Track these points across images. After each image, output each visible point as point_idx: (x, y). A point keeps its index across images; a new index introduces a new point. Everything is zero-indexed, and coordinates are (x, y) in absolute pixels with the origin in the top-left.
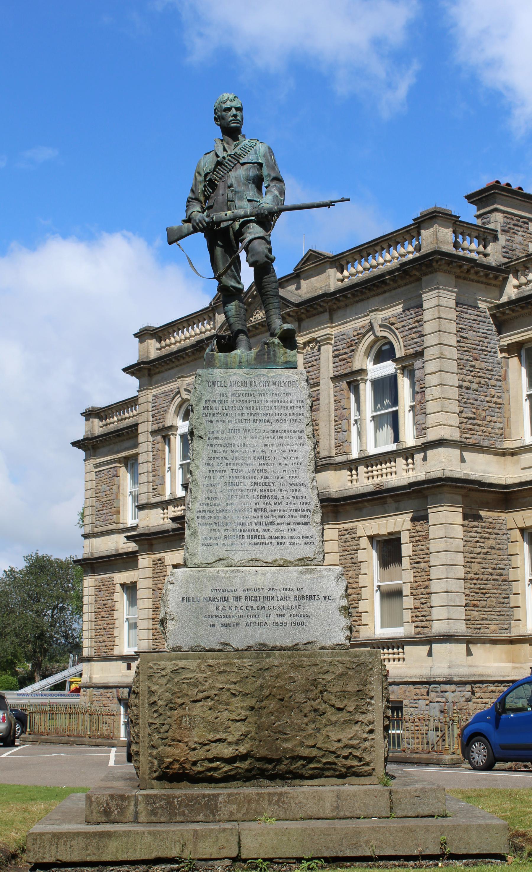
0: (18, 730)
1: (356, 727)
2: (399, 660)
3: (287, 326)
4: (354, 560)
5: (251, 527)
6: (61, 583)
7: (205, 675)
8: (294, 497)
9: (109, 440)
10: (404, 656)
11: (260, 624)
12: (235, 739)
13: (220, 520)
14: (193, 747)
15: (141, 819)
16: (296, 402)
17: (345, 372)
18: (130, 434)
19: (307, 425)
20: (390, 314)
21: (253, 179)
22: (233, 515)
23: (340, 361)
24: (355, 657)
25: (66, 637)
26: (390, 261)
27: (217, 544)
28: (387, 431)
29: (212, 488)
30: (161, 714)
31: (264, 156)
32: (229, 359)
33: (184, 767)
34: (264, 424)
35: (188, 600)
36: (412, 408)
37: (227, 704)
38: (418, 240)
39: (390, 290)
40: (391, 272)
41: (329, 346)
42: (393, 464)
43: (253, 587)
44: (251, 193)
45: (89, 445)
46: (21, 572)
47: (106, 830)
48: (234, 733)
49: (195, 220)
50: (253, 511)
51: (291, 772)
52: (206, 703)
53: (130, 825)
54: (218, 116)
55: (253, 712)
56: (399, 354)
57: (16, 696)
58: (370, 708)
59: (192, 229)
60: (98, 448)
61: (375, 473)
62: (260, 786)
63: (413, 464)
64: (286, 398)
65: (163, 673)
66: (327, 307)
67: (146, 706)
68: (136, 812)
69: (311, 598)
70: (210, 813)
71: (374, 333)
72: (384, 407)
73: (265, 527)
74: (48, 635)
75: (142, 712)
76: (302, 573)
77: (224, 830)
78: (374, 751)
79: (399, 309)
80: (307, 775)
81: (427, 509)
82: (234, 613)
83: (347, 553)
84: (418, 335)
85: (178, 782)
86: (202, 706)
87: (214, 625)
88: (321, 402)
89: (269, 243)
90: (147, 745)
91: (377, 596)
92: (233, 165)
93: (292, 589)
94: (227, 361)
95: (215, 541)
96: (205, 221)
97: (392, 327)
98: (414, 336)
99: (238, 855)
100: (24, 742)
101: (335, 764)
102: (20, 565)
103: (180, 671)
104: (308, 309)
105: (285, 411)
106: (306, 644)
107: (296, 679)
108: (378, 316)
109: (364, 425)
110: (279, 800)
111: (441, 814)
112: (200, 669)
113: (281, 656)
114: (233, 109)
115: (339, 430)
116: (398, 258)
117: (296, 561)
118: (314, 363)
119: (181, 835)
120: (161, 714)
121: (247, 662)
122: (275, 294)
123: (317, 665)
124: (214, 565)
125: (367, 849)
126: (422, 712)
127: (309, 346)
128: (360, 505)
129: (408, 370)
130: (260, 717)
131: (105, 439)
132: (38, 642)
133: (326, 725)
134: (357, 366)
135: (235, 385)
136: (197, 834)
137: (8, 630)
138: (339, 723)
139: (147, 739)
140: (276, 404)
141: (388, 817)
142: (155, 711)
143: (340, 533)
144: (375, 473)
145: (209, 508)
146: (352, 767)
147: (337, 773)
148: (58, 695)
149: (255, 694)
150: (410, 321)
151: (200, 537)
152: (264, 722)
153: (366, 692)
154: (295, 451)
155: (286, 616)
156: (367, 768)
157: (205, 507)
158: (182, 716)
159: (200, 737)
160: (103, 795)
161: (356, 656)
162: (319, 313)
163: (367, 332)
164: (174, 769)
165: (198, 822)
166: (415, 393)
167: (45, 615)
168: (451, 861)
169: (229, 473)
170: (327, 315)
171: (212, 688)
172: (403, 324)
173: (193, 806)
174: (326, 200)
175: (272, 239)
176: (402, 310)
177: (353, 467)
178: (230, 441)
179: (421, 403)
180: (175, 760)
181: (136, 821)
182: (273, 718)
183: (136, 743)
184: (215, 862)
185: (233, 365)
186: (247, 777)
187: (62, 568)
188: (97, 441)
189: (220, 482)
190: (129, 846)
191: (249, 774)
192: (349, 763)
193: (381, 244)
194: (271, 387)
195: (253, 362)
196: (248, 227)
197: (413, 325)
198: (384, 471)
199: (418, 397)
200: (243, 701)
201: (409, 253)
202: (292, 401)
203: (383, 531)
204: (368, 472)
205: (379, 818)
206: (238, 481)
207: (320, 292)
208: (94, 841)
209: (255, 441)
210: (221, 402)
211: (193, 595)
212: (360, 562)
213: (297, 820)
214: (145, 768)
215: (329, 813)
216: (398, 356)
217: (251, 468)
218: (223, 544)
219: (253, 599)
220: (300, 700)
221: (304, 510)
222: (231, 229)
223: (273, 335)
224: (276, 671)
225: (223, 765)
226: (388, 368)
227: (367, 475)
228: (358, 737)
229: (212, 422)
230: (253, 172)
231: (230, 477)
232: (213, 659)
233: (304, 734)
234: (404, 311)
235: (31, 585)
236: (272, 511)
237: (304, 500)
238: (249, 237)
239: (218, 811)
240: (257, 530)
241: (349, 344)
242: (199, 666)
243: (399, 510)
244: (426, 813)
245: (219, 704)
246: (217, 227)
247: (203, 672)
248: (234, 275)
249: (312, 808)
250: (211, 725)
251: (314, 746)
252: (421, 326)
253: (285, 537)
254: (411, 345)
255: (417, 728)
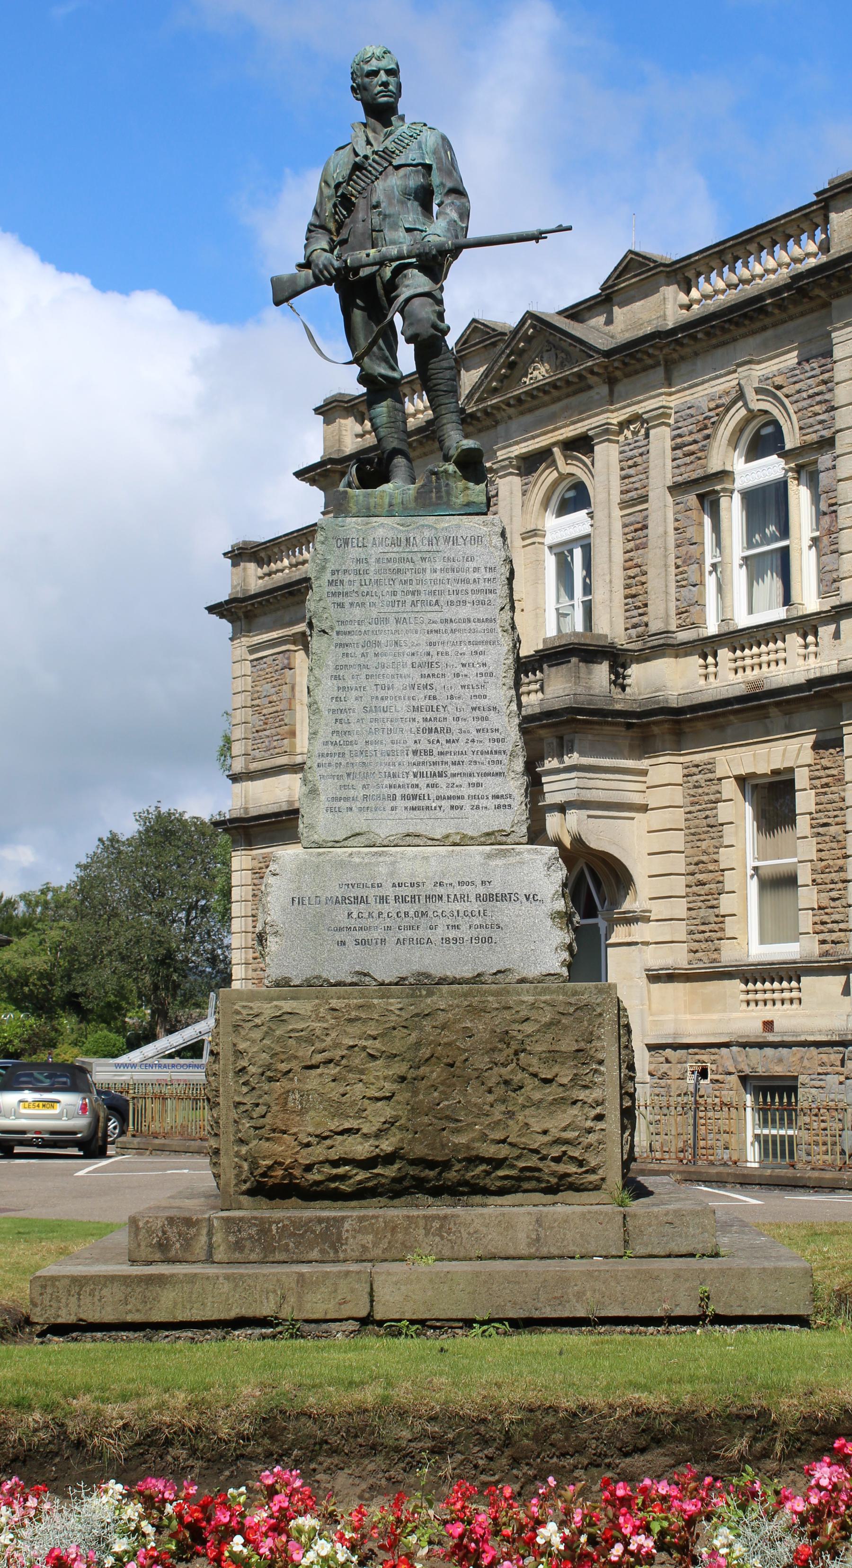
0: (115, 1128)
1: (575, 1111)
2: (792, 1003)
3: (469, 443)
4: (711, 821)
5: (406, 781)
6: (203, 861)
7: (325, 1025)
8: (478, 731)
9: (269, 602)
10: (801, 995)
11: (419, 942)
12: (374, 1129)
13: (356, 769)
14: (305, 1141)
15: (218, 1256)
16: (483, 570)
17: (694, 476)
18: (295, 592)
19: (502, 609)
20: (775, 368)
21: (415, 193)
22: (378, 760)
23: (685, 455)
24: (573, 995)
25: (213, 960)
26: (774, 271)
27: (351, 809)
28: (771, 584)
29: (343, 716)
30: (254, 1088)
31: (435, 152)
32: (372, 501)
33: (291, 1174)
34: (429, 608)
35: (301, 901)
36: (815, 541)
37: (362, 1072)
38: (825, 231)
39: (774, 325)
40: (775, 292)
41: (664, 428)
42: (780, 644)
43: (409, 881)
44: (411, 216)
45: (239, 612)
46: (129, 843)
47: (157, 1272)
48: (372, 1119)
49: (317, 265)
50: (411, 754)
51: (466, 1183)
52: (326, 1071)
53: (200, 1265)
54: (358, 85)
55: (403, 1085)
56: (791, 441)
57: (114, 1069)
58: (598, 1079)
59: (312, 280)
60: (255, 616)
61: (748, 662)
62: (417, 1206)
63: (817, 645)
64: (467, 565)
65: (258, 1021)
66: (661, 357)
67: (231, 1075)
68: (210, 1246)
69: (504, 897)
70: (330, 1247)
71: (746, 405)
72: (766, 541)
73: (431, 781)
74: (180, 957)
75: (224, 1085)
76: (489, 856)
77: (347, 1273)
78: (604, 1149)
79: (791, 359)
80: (493, 1188)
81: (841, 727)
82: (377, 923)
83: (698, 807)
84: (824, 407)
85: (283, 1198)
86: (321, 1075)
87: (343, 943)
88: (650, 531)
89: (440, 302)
90: (232, 1138)
91: (753, 885)
92: (381, 169)
93: (473, 883)
94: (369, 503)
95: (348, 804)
96: (333, 266)
97: (778, 393)
98: (817, 408)
99: (369, 1314)
100: (124, 1149)
101: (539, 1170)
102: (129, 828)
103: (285, 1017)
104: (627, 360)
105: (464, 587)
106: (495, 974)
107: (475, 1031)
108: (754, 373)
109: (728, 573)
110: (442, 1226)
111: (709, 1252)
112: (317, 1015)
113: (452, 994)
114: (382, 72)
115: (683, 583)
116: (788, 265)
117: (481, 836)
118: (639, 460)
119: (278, 1281)
120: (254, 1088)
121: (394, 1004)
122: (449, 388)
123: (510, 1008)
124: (346, 843)
125: (578, 1306)
126: (832, 1096)
127: (628, 429)
128: (721, 720)
129: (807, 473)
130: (415, 1093)
131: (268, 600)
132: (163, 972)
133: (524, 1107)
134: (715, 466)
135: (381, 543)
136: (303, 1280)
137: (105, 949)
138: (545, 1104)
139: (232, 1129)
140: (450, 575)
141: (621, 1257)
142: (243, 1084)
143: (686, 771)
144: (748, 662)
145: (337, 749)
146: (568, 1175)
147: (543, 1185)
148: (189, 1066)
149: (407, 1055)
150: (810, 382)
151: (323, 798)
152: (422, 1101)
153: (591, 1053)
154: (481, 653)
155: (463, 928)
156: (592, 1178)
157: (331, 747)
158: (288, 1092)
159: (318, 1125)
160: (157, 1218)
161: (575, 993)
162: (646, 369)
163: (734, 402)
164: (275, 1177)
165: (310, 1262)
166: (820, 514)
167: (174, 921)
168: (717, 1327)
169: (371, 691)
170: (660, 372)
171: (336, 1045)
172: (797, 387)
173: (302, 1236)
174: (531, 227)
175: (446, 296)
176: (796, 360)
177: (708, 650)
178: (373, 638)
179: (830, 533)
180: (275, 1163)
181: (209, 1260)
182: (436, 1094)
183: (216, 1135)
184: (333, 1325)
185: (378, 511)
186: (396, 1191)
187: (204, 834)
188: (253, 604)
189: (356, 706)
190: (194, 1299)
191: (397, 1187)
192: (562, 1168)
193: (758, 240)
194: (442, 547)
195: (412, 505)
196: (405, 276)
197: (816, 390)
198: (764, 658)
199: (826, 521)
200: (388, 1067)
201: (808, 255)
202: (476, 570)
203: (763, 768)
204: (735, 660)
205: (606, 1257)
206: (386, 703)
207: (649, 330)
208: (139, 1290)
209: (414, 637)
210: (358, 572)
211: (309, 894)
212: (722, 825)
213: (471, 1259)
214: (229, 1175)
215: (524, 1250)
216: (788, 447)
217: (407, 682)
218: (361, 809)
219: (408, 899)
220: (481, 1066)
221: (496, 752)
222: (378, 278)
223: (447, 459)
224: (441, 1017)
225: (354, 1172)
226: (771, 468)
227: (733, 665)
228: (577, 1126)
229: (343, 607)
230: (415, 181)
231: (372, 698)
232: (339, 998)
233: (487, 1121)
234: (799, 363)
235: (147, 866)
236: (441, 753)
237: (496, 735)
238: (405, 293)
239: (342, 1244)
240: (417, 786)
241: (701, 425)
242: (316, 1010)
243: (790, 729)
244: (683, 1250)
245: (350, 1071)
246: (354, 276)
247: (323, 1019)
248: (384, 355)
249: (495, 1241)
250: (335, 1105)
251: (504, 1141)
252: (831, 390)
253: (463, 797)
254: (811, 426)
255: (823, 1125)
